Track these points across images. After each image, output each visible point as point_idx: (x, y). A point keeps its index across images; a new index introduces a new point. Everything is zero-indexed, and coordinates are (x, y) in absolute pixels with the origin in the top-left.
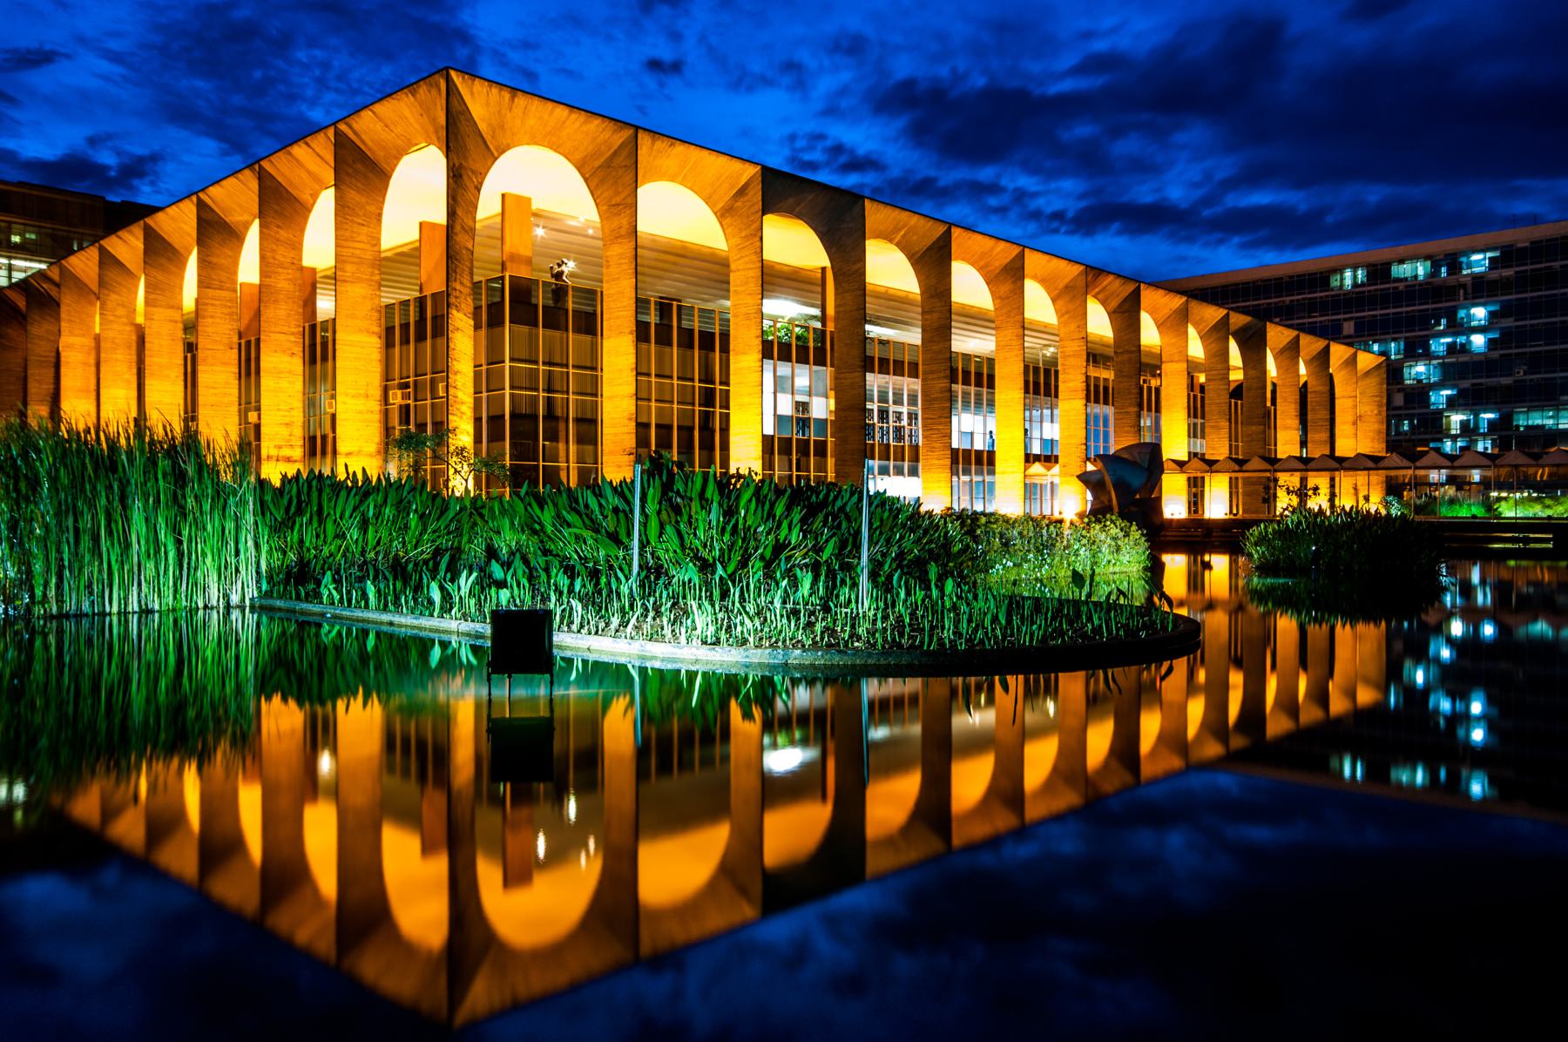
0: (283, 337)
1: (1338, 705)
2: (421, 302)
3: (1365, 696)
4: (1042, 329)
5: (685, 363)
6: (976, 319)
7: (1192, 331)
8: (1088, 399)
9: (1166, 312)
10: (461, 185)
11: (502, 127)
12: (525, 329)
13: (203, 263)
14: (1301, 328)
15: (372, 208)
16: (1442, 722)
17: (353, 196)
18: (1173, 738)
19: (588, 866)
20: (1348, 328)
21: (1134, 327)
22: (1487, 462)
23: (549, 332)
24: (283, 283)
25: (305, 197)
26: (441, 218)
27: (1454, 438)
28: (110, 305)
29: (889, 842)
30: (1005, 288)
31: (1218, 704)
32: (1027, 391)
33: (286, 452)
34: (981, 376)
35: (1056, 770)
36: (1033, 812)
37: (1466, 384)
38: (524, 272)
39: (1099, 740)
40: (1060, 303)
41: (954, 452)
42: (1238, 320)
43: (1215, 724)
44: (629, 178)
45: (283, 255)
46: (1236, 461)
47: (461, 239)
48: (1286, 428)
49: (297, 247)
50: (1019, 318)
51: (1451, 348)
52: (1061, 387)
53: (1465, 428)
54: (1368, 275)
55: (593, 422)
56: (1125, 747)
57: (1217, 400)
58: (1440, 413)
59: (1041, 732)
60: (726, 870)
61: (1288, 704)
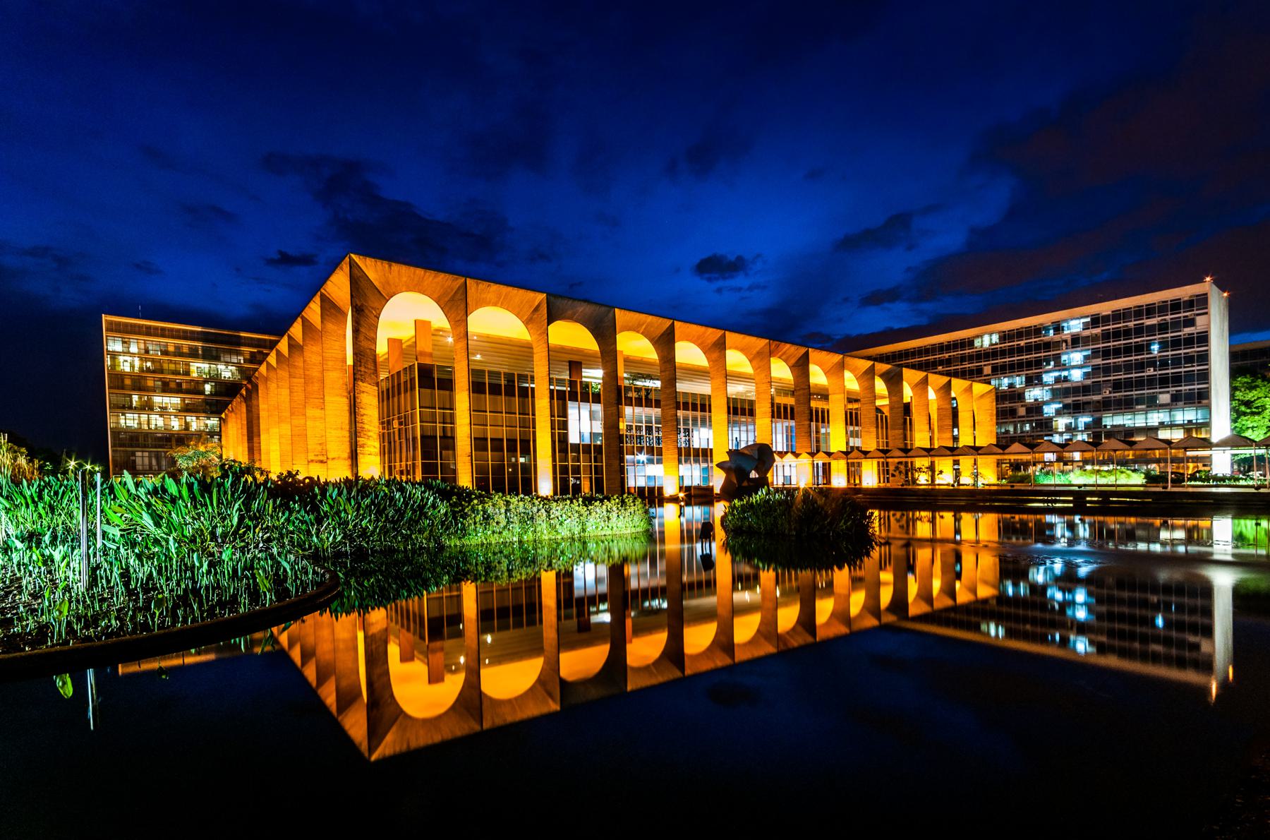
1: (963, 597)
3: (984, 592)
5: (509, 404)
6: (695, 373)
8: (773, 417)
9: (830, 365)
11: (388, 283)
12: (429, 391)
14: (948, 374)
16: (1057, 607)
18: (841, 615)
19: (661, 638)
20: (987, 370)
21: (806, 374)
22: (1090, 447)
23: (442, 392)
27: (1061, 434)
29: (645, 669)
30: (715, 355)
31: (874, 597)
32: (729, 413)
34: (702, 405)
35: (864, 607)
36: (740, 656)
37: (1069, 400)
38: (428, 361)
39: (788, 617)
41: (680, 449)
42: (882, 367)
43: (872, 607)
44: (463, 306)
46: (882, 451)
48: (921, 431)
51: (1058, 380)
52: (758, 411)
53: (1069, 429)
54: (1000, 338)
55: (453, 438)
56: (807, 620)
57: (867, 416)
58: (1050, 419)
59: (747, 609)
60: (541, 681)
61: (926, 595)
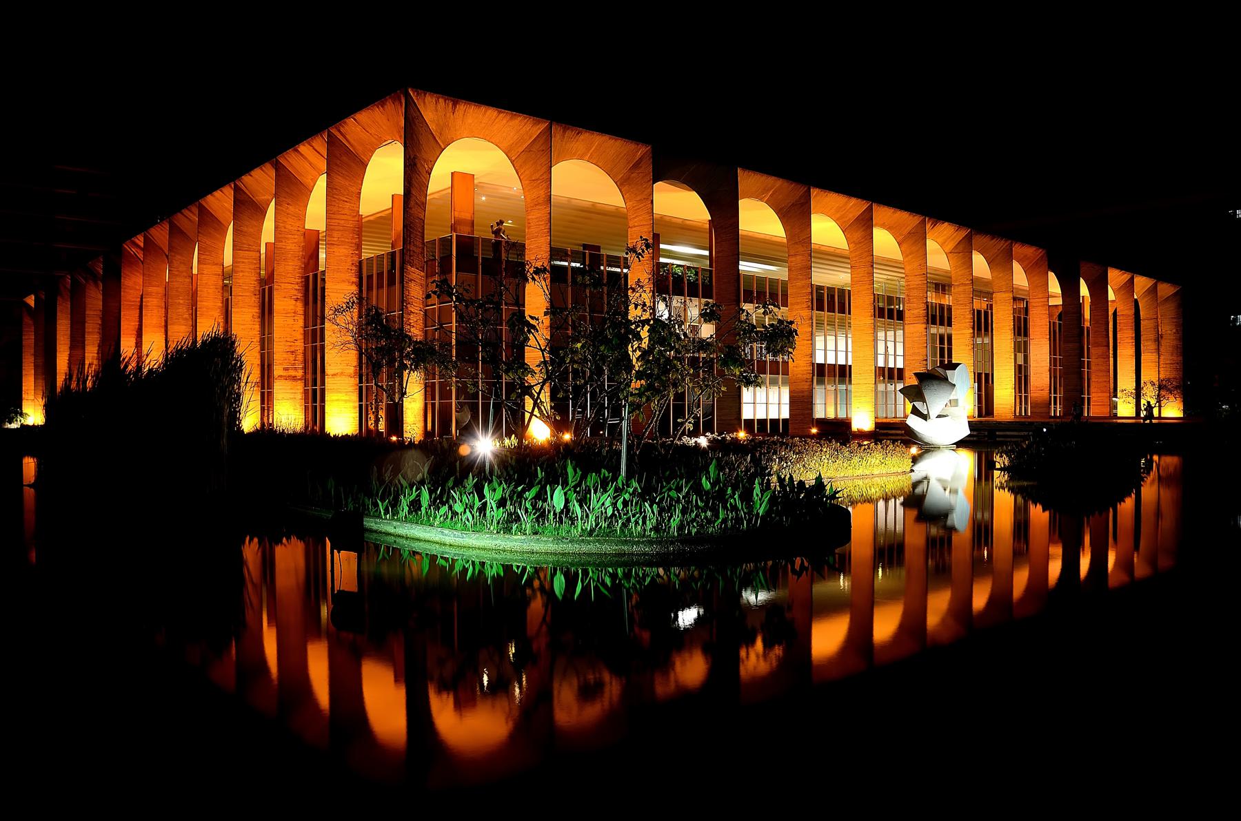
0: (290, 286)
2: (393, 255)
4: (889, 264)
6: (831, 257)
7: (1017, 267)
10: (415, 172)
13: (236, 231)
15: (353, 189)
17: (339, 180)
24: (294, 246)
25: (307, 180)
26: (400, 190)
28: (175, 264)
33: (292, 373)
40: (905, 245)
45: (291, 224)
47: (415, 211)
49: (302, 218)
50: (869, 259)
